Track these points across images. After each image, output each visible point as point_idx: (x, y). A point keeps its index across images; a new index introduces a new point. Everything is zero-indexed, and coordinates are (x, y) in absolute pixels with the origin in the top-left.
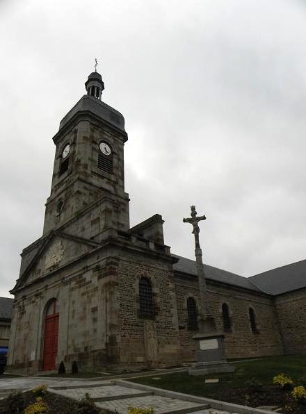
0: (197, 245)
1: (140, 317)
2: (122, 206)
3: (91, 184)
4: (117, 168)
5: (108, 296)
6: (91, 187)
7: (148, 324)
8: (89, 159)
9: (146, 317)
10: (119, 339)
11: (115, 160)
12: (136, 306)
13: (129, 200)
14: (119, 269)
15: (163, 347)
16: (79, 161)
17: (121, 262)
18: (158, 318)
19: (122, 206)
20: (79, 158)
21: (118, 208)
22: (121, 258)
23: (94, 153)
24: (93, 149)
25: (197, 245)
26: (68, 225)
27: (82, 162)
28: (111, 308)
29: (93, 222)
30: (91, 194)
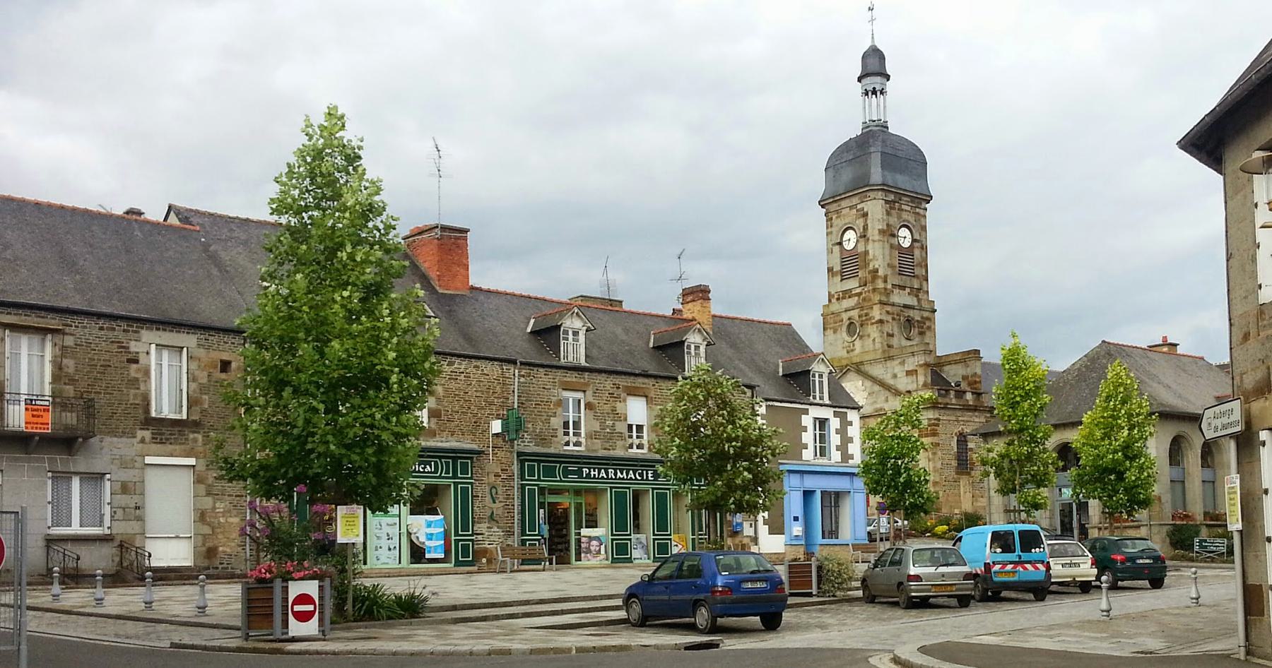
0: (537, 628)
1: (957, 473)
2: (928, 323)
3: (893, 305)
4: (920, 265)
5: (931, 456)
6: (895, 308)
7: (964, 481)
8: (888, 264)
9: (962, 474)
10: (941, 494)
11: (917, 252)
12: (954, 463)
13: (928, 199)
14: (940, 429)
15: (977, 501)
16: (877, 271)
17: (941, 422)
18: (973, 473)
19: (928, 323)
20: (877, 266)
21: (922, 327)
22: (941, 417)
23: (893, 251)
24: (892, 246)
25: (537, 628)
26: (871, 362)
27: (881, 273)
28: (934, 467)
29: (909, 373)
30: (893, 319)
